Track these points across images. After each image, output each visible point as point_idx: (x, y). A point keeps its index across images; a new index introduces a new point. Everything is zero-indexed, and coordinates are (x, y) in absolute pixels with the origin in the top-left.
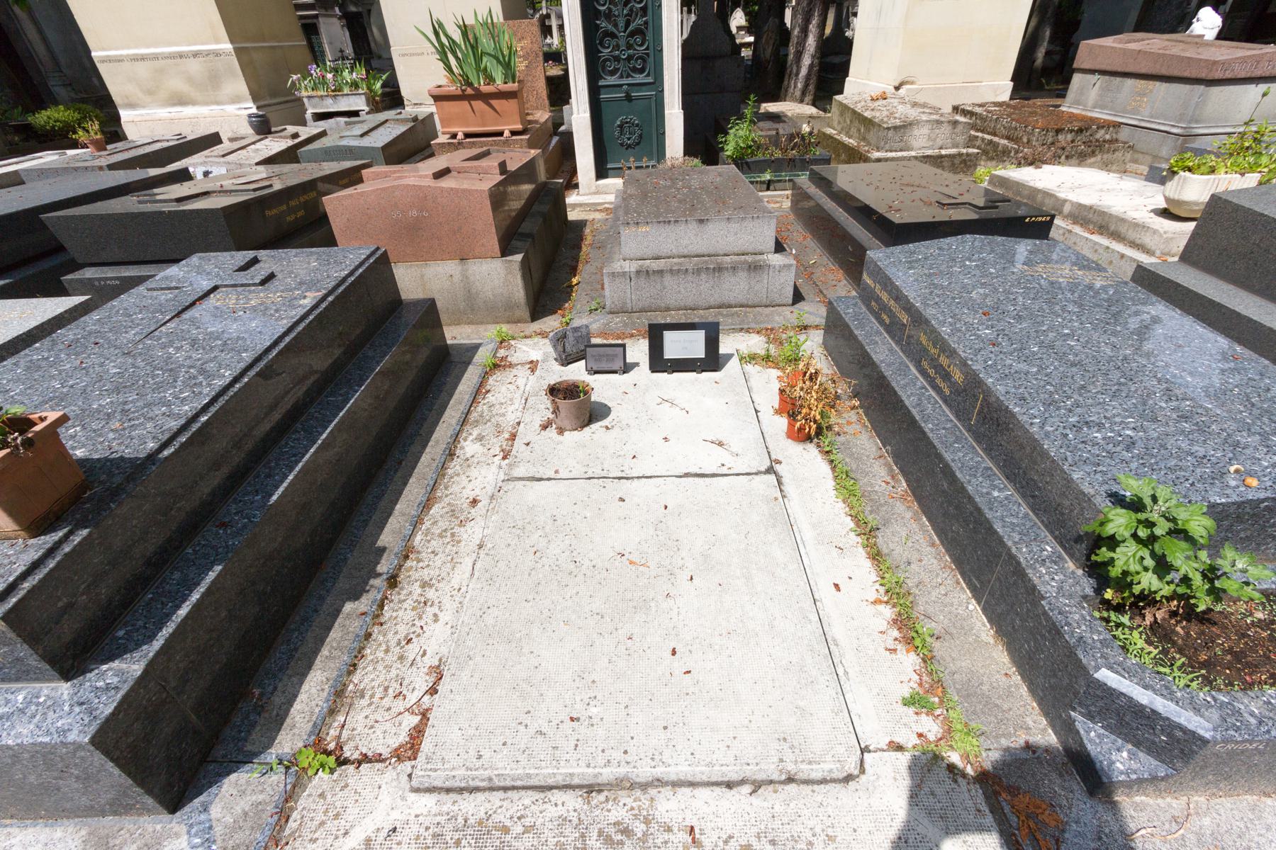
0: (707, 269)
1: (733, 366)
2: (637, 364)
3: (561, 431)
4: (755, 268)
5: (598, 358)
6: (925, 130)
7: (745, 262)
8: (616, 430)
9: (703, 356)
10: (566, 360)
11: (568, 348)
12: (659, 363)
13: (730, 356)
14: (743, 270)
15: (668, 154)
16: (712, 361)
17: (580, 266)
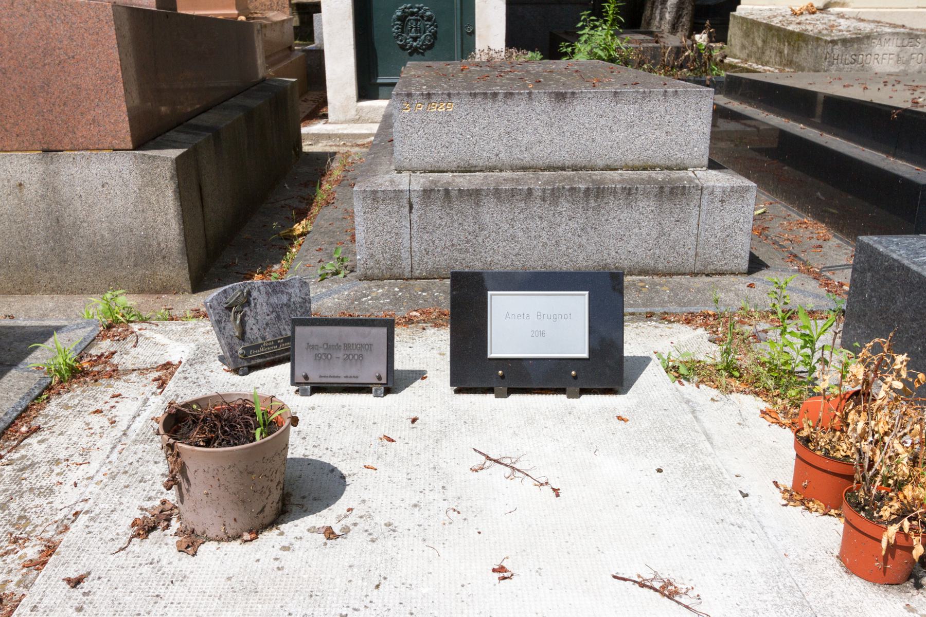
0: (573, 190)
1: (652, 383)
2: (420, 375)
3: (191, 542)
4: (673, 193)
5: (324, 353)
6: (892, 47)
7: (650, 181)
8: (356, 539)
9: (585, 355)
10: (247, 361)
11: (254, 331)
12: (477, 370)
13: (642, 363)
14: (646, 194)
15: (480, 44)
16: (603, 370)
17: (315, 210)
